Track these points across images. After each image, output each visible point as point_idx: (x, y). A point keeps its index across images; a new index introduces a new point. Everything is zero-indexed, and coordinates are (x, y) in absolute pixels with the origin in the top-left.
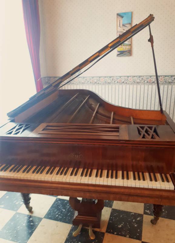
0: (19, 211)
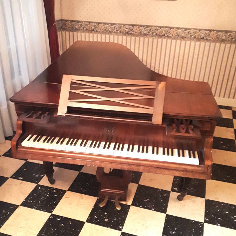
0: (40, 183)
